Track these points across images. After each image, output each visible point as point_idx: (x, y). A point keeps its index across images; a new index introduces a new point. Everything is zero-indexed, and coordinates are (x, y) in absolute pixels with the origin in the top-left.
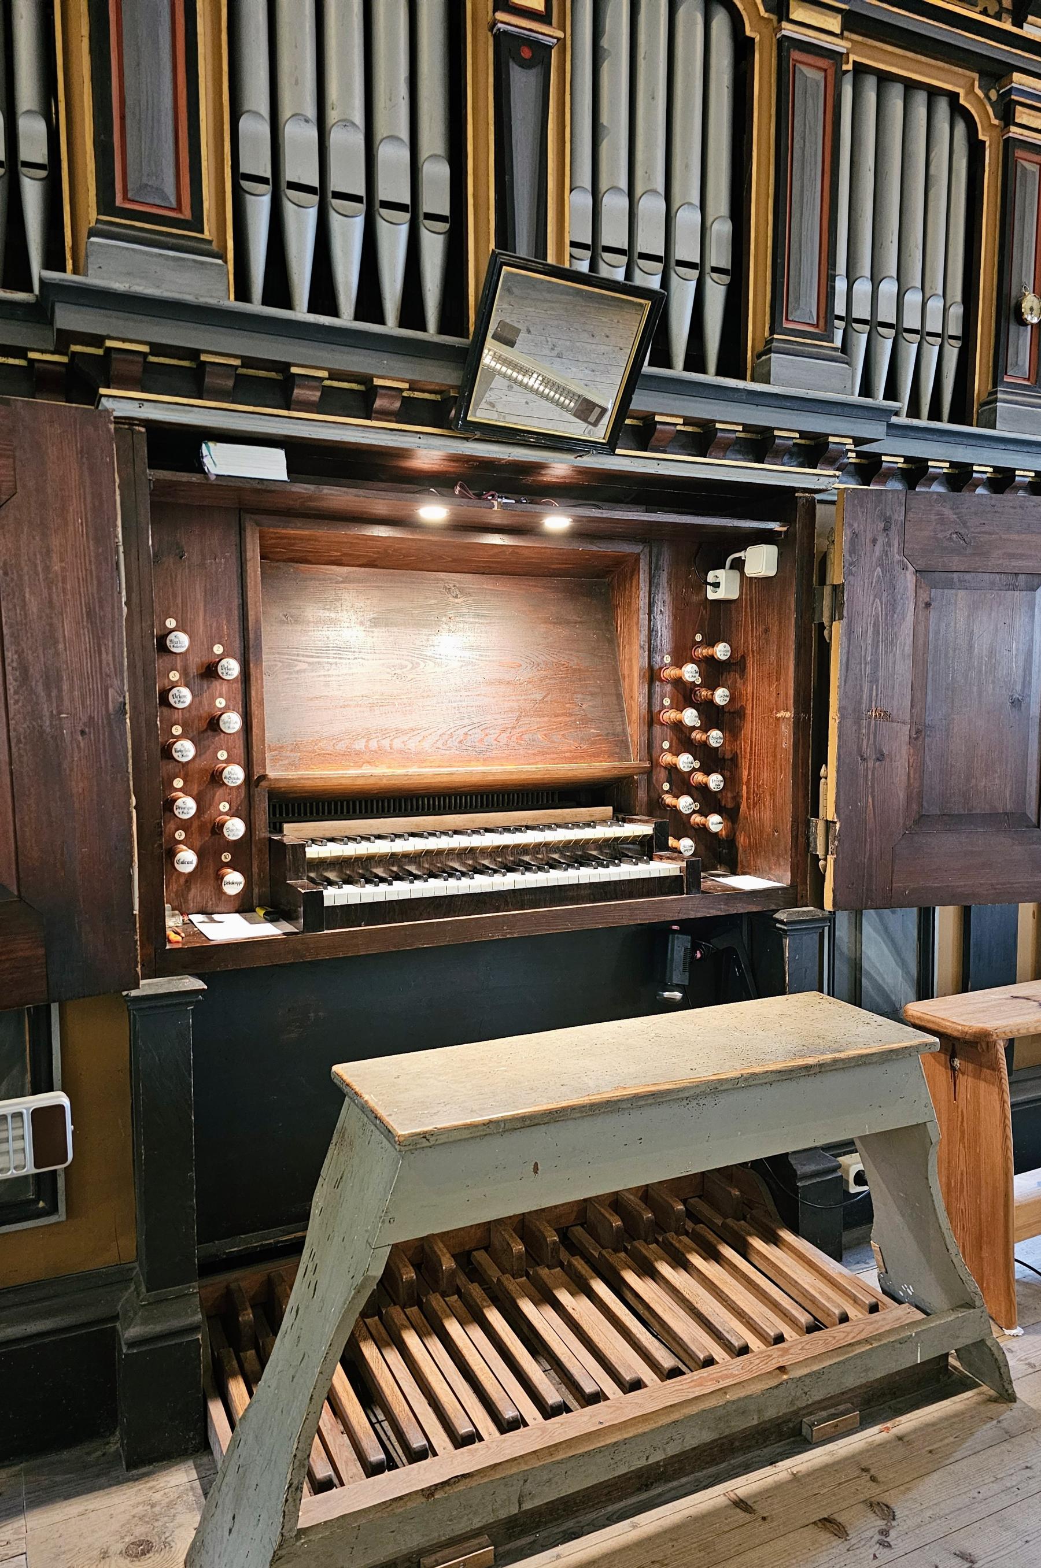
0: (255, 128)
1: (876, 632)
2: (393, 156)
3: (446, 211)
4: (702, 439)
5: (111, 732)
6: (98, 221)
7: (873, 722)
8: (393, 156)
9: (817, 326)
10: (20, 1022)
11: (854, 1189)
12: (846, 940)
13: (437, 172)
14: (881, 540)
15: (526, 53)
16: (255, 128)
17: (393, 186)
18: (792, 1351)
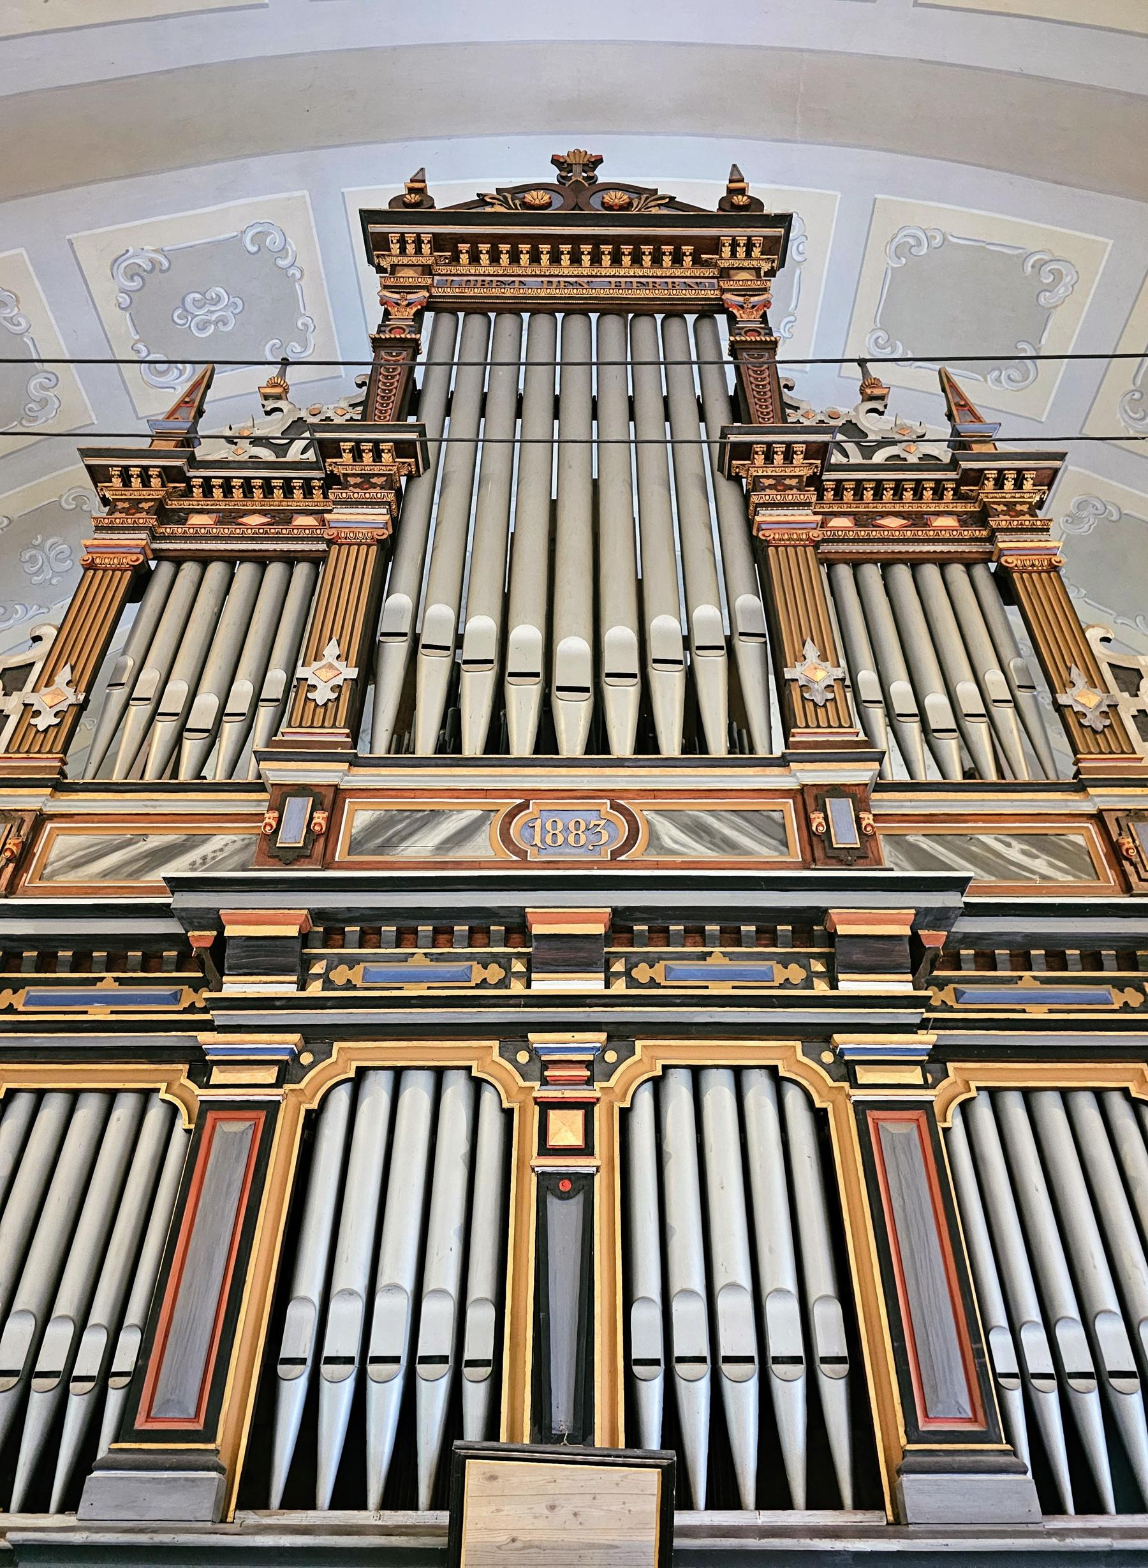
0: (647, 1317)
2: (782, 1314)
3: (844, 1353)
6: (110, 1451)
8: (782, 1314)
9: (974, 1420)
13: (828, 1317)
15: (565, 1186)
16: (647, 1317)
17: (785, 1339)
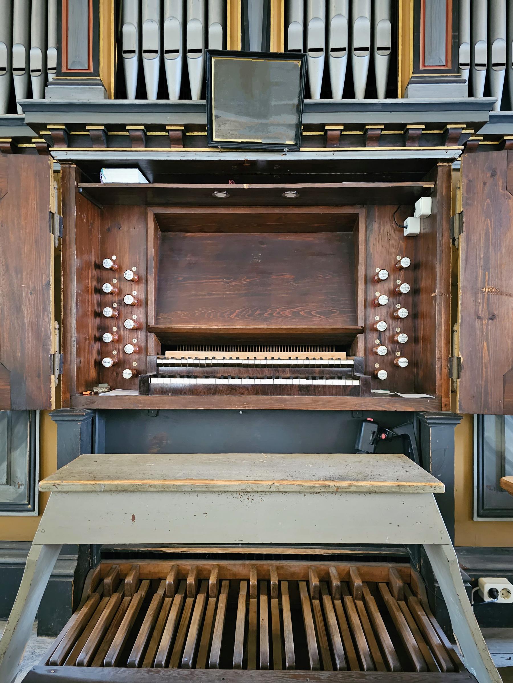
1: (487, 239)
4: (361, 135)
5: (43, 294)
7: (486, 295)
10: (26, 424)
11: (487, 599)
12: (494, 440)
14: (490, 181)
18: (367, 677)
